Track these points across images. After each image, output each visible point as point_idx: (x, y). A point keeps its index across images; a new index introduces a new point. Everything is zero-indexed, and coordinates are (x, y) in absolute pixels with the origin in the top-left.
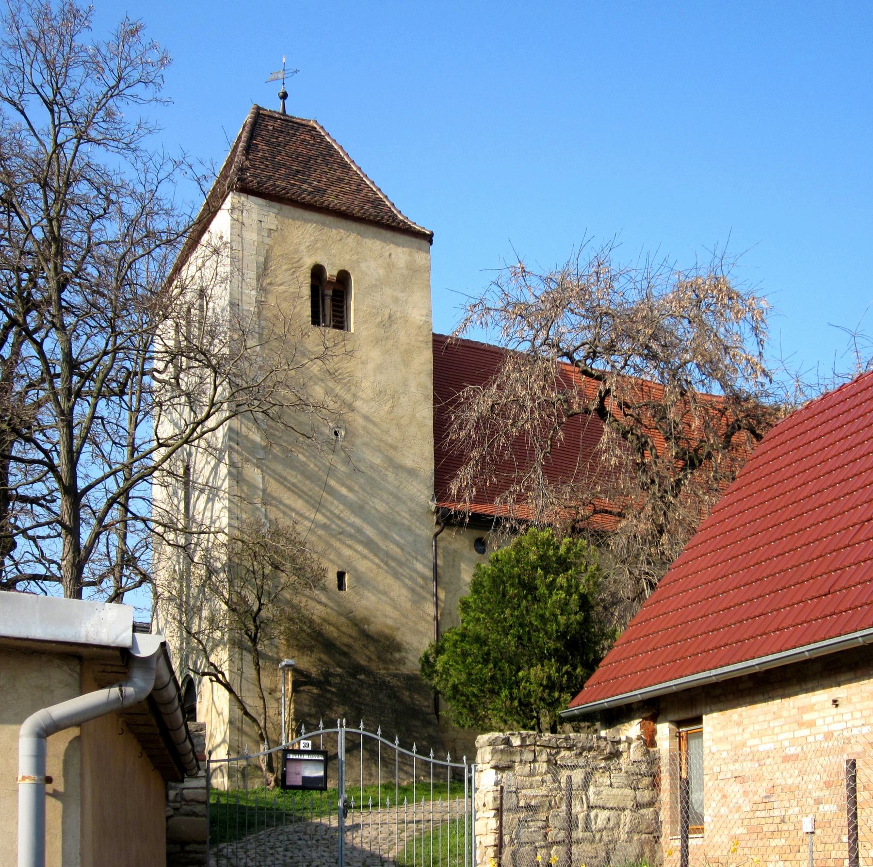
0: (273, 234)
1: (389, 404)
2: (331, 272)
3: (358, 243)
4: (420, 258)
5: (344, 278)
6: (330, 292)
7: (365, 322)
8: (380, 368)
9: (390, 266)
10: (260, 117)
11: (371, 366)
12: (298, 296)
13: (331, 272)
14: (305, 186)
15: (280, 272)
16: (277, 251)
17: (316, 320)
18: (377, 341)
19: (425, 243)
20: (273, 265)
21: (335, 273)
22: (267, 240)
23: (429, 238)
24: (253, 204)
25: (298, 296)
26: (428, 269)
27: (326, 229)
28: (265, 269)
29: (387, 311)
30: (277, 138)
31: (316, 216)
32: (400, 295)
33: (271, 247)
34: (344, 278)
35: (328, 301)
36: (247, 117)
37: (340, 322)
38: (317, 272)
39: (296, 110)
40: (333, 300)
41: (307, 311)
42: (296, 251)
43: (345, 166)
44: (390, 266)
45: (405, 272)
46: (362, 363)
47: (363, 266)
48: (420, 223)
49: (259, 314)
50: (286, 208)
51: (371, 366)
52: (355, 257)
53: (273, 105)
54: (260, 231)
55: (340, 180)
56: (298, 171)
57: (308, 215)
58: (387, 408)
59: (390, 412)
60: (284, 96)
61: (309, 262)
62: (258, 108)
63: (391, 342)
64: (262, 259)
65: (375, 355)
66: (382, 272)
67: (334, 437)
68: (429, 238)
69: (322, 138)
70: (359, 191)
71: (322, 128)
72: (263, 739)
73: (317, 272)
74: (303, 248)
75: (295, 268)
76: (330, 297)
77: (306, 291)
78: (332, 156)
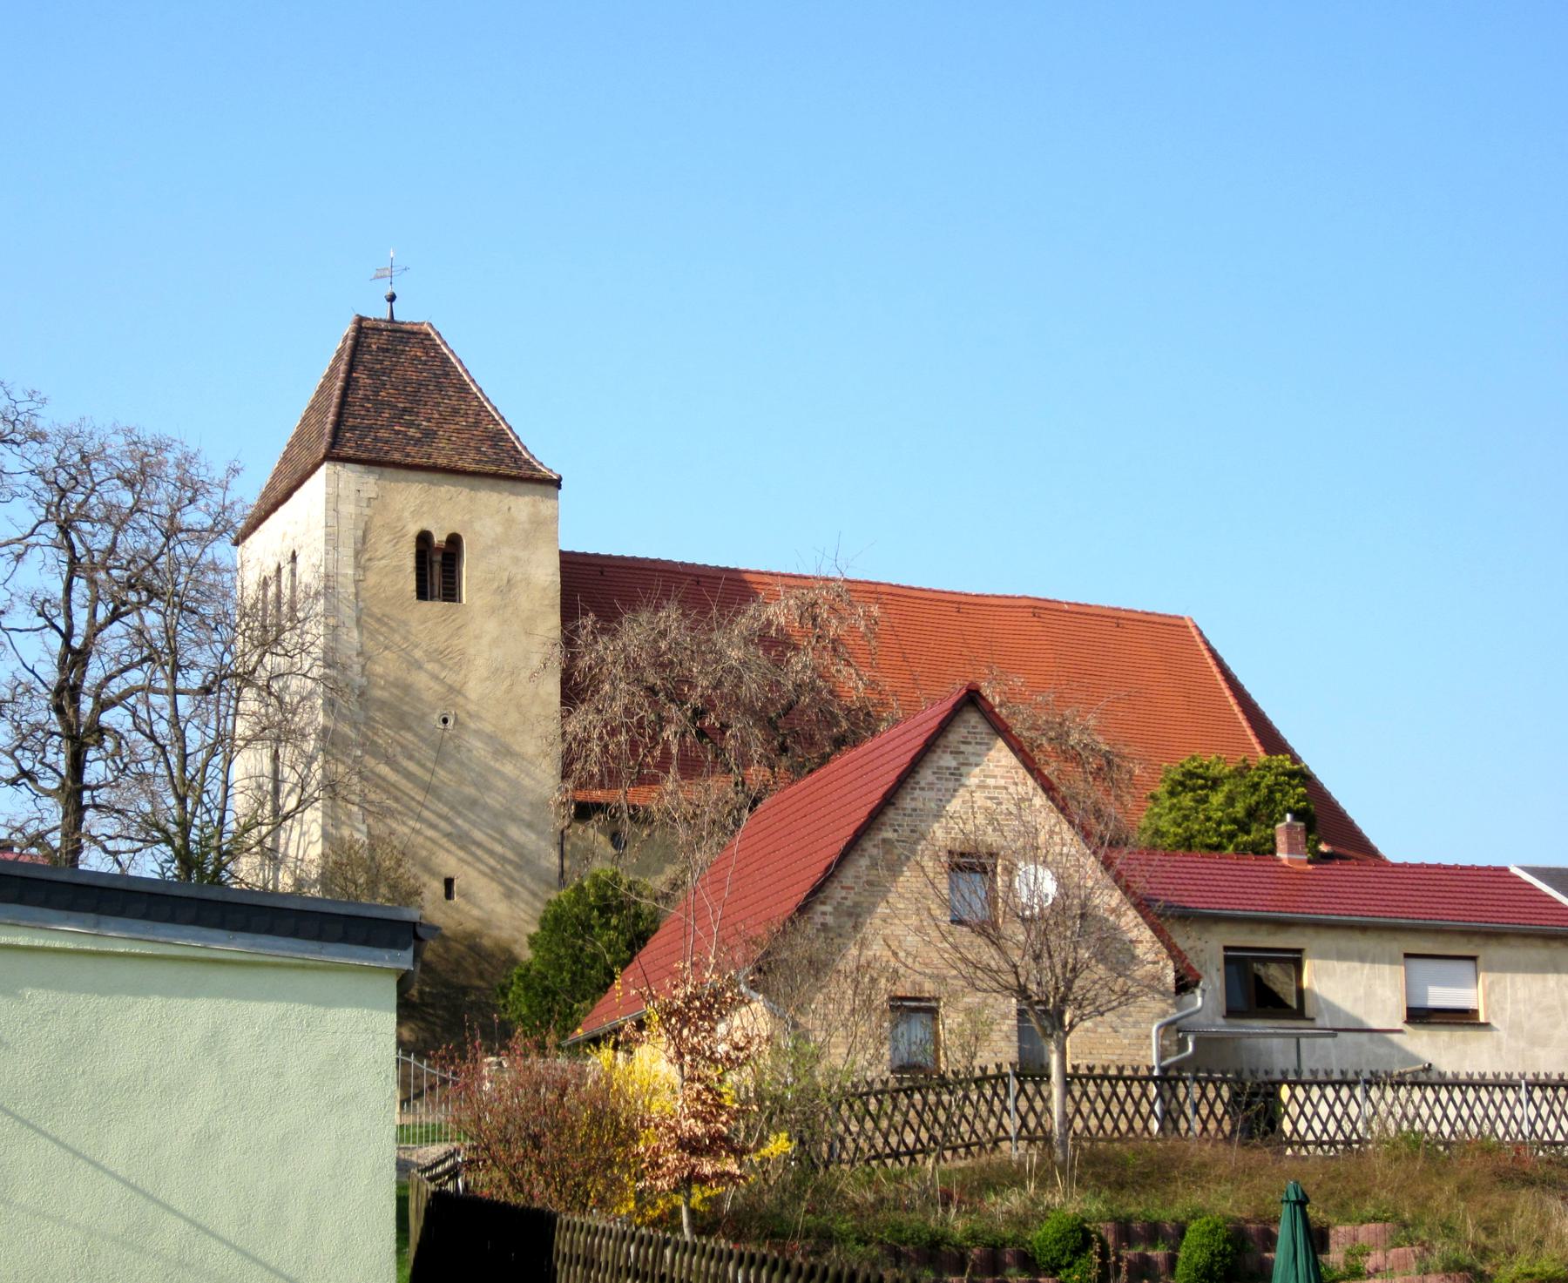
0: (373, 503)
1: (507, 683)
2: (439, 538)
3: (472, 500)
4: (545, 507)
5: (454, 541)
6: (438, 558)
7: (480, 590)
8: (496, 642)
9: (509, 522)
10: (363, 330)
11: (485, 640)
12: (399, 569)
13: (439, 538)
14: (412, 432)
15: (382, 544)
16: (378, 521)
17: (422, 594)
18: (493, 611)
19: (552, 489)
20: (372, 538)
21: (444, 538)
22: (367, 511)
23: (557, 483)
24: (349, 475)
25: (399, 569)
26: (555, 519)
27: (434, 488)
28: (364, 543)
29: (505, 577)
30: (381, 362)
31: (423, 475)
32: (523, 555)
33: (371, 518)
34: (454, 541)
35: (437, 569)
36: (347, 328)
37: (451, 592)
38: (424, 538)
39: (405, 314)
40: (443, 565)
41: (412, 585)
42: (399, 519)
43: (463, 389)
44: (509, 522)
45: (527, 526)
46: (476, 637)
47: (477, 526)
48: (547, 458)
49: (357, 595)
50: (388, 471)
51: (485, 640)
52: (467, 517)
53: (377, 311)
54: (358, 500)
55: (455, 411)
56: (404, 410)
57: (412, 475)
58: (504, 687)
59: (509, 690)
60: (392, 298)
61: (413, 529)
62: (361, 319)
63: (510, 610)
64: (360, 533)
65: (491, 627)
66: (499, 529)
67: (441, 726)
68: (557, 483)
69: (436, 347)
70: (477, 423)
71: (438, 334)
72: (499, 591)
73: (424, 538)
74: (406, 514)
75: (398, 538)
76: (438, 568)
77: (410, 563)
78: (447, 375)
